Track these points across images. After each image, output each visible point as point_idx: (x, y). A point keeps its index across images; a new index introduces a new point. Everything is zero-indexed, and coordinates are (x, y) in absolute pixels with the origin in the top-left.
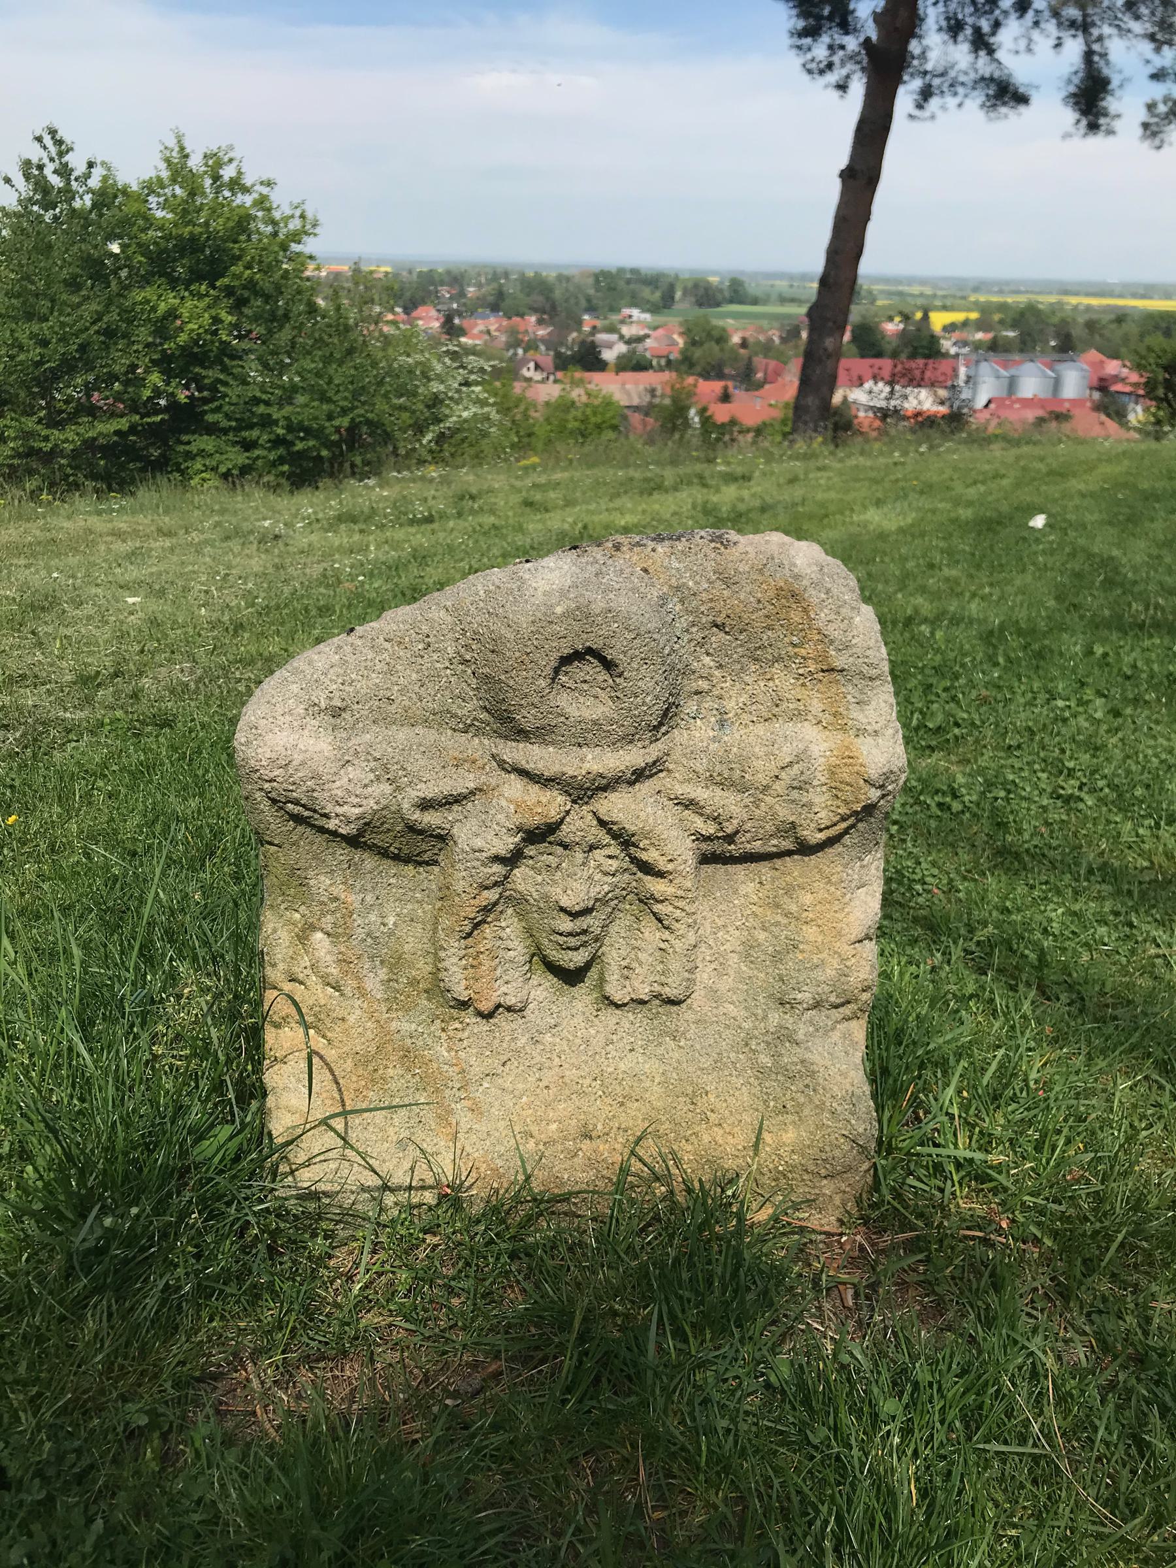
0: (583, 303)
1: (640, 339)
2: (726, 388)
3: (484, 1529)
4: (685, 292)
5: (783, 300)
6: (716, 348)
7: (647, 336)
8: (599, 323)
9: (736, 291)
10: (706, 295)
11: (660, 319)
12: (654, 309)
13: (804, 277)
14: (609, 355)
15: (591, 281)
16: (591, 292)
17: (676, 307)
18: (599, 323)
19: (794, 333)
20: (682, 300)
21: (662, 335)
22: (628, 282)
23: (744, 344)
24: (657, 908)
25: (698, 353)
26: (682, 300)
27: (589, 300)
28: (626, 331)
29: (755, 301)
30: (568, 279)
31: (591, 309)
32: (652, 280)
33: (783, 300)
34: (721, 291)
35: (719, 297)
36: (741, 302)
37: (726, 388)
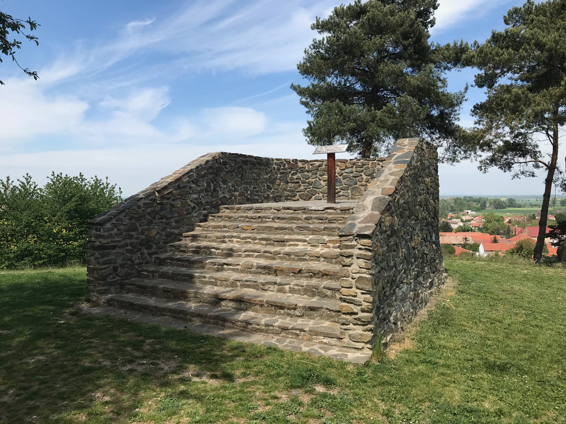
0: (450, 209)
1: (469, 221)
2: (495, 238)
3: (93, 345)
4: (491, 204)
5: (532, 205)
6: (497, 224)
7: (473, 219)
8: (454, 215)
9: (511, 203)
10: (498, 205)
11: (479, 213)
12: (477, 210)
13: (537, 197)
14: (454, 226)
15: (453, 201)
16: (453, 205)
17: (487, 209)
18: (454, 215)
19: (534, 217)
20: (489, 207)
21: (474, 218)
22: (468, 201)
23: (510, 222)
24: (5, 183)
25: (489, 225)
26: (489, 207)
27: (452, 208)
28: (464, 218)
29: (520, 206)
30: (445, 201)
31: (453, 210)
32: (478, 200)
33: (532, 205)
34: (505, 203)
35: (504, 205)
36: (514, 207)
37: (495, 238)
